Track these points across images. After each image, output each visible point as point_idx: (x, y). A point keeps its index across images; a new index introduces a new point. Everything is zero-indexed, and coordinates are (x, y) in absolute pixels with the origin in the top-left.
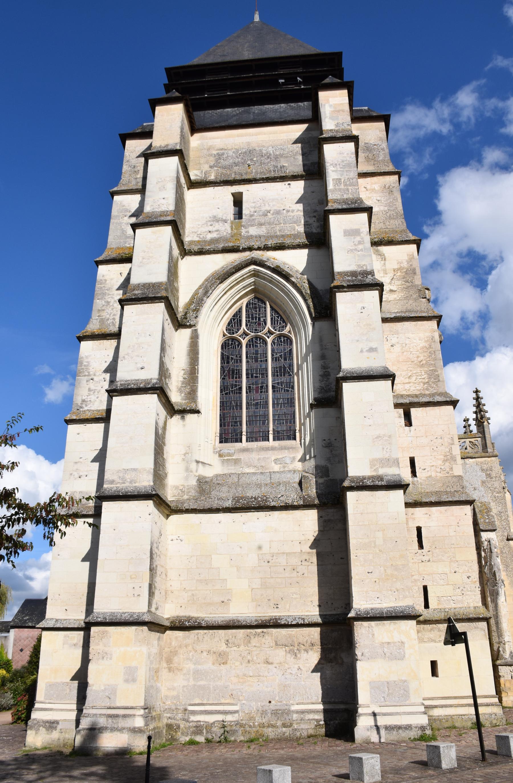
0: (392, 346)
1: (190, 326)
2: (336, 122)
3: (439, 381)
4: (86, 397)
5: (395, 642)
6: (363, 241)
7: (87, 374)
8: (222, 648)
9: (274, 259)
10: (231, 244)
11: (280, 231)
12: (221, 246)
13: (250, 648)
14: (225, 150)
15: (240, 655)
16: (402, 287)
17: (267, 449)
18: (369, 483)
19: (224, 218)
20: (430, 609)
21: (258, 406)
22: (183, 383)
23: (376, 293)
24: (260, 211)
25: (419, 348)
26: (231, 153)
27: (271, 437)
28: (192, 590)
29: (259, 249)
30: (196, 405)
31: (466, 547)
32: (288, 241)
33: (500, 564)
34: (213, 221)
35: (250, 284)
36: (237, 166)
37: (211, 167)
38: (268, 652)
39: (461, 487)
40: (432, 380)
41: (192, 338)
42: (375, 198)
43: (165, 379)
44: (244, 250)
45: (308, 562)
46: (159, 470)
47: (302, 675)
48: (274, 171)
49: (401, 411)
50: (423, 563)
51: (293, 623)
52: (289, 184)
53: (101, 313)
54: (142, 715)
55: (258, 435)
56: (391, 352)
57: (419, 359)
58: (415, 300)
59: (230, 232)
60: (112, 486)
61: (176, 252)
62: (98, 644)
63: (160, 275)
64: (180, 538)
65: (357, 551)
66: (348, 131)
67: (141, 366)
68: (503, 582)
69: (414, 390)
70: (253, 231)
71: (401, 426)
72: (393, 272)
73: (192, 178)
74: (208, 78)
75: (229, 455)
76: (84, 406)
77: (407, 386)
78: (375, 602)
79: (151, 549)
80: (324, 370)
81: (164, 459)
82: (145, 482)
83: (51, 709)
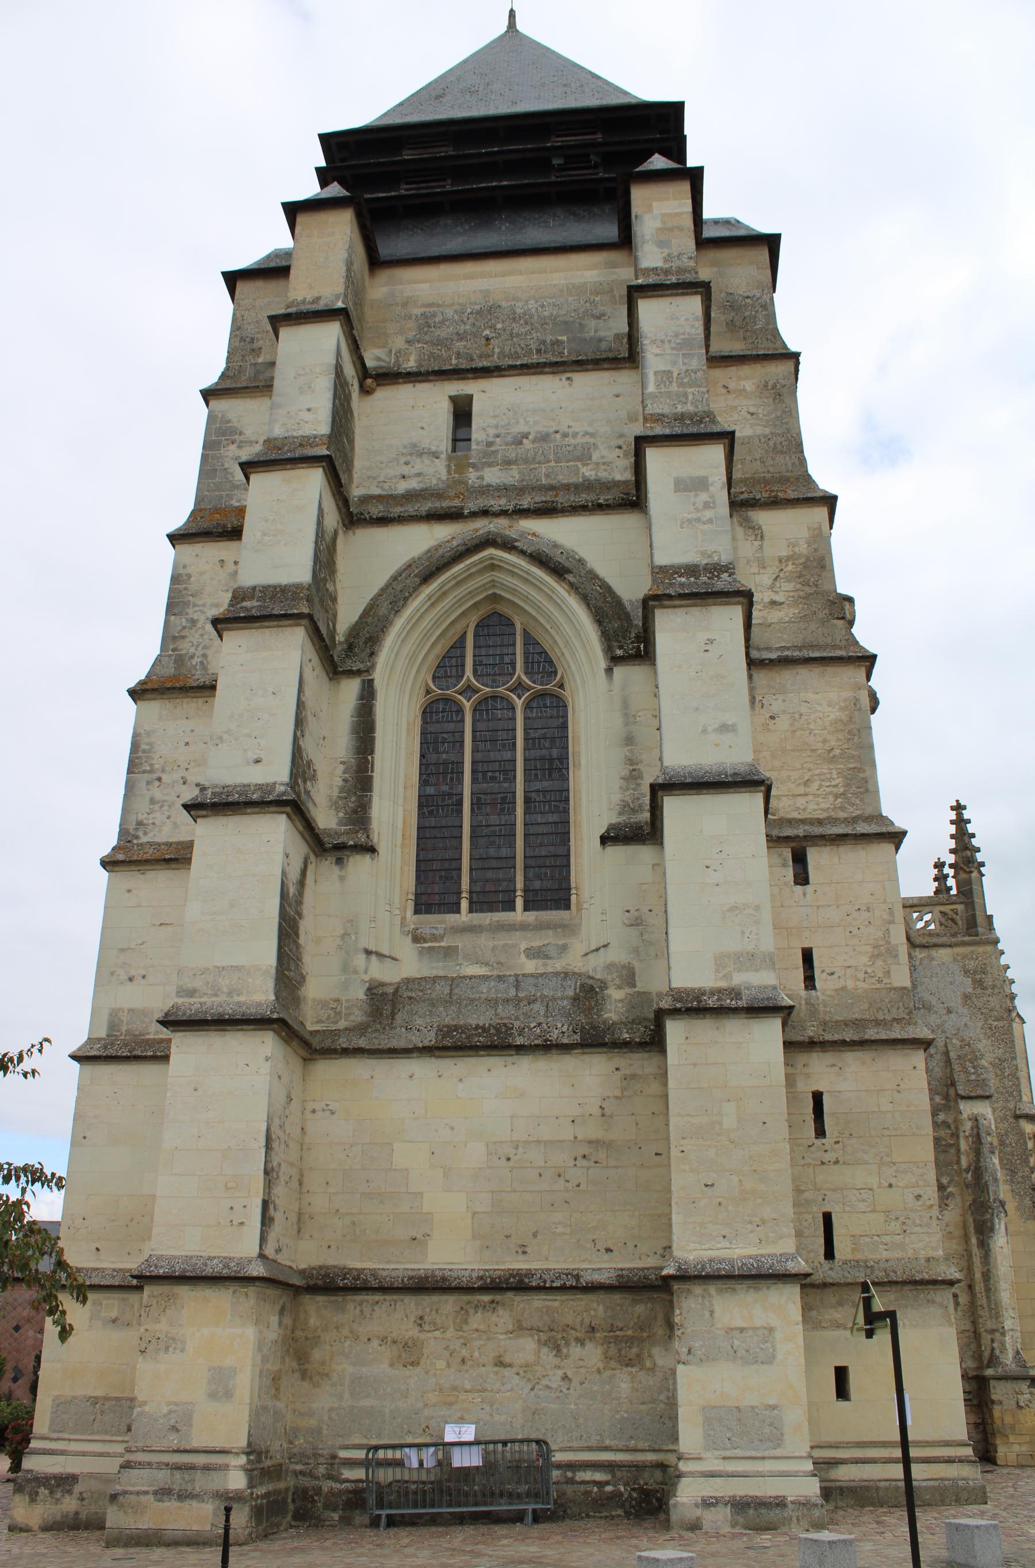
0: (772, 718)
1: (359, 672)
2: (666, 251)
3: (867, 791)
4: (145, 815)
5: (757, 1328)
6: (714, 503)
7: (148, 768)
8: (411, 1333)
9: (534, 534)
10: (446, 504)
11: (547, 476)
12: (425, 507)
13: (465, 1334)
14: (439, 306)
15: (447, 1348)
16: (796, 594)
17: (512, 928)
18: (711, 1002)
19: (434, 449)
20: (836, 1260)
21: (492, 836)
22: (342, 790)
23: (736, 613)
24: (508, 434)
25: (827, 724)
26: (449, 313)
27: (519, 903)
28: (353, 1214)
29: (504, 513)
30: (368, 837)
31: (914, 1134)
32: (563, 499)
33: (998, 1167)
34: (411, 454)
35: (484, 585)
36: (461, 339)
37: (409, 342)
38: (503, 1343)
39: (907, 1011)
40: (854, 789)
41: (362, 697)
42: (745, 409)
43: (305, 782)
44: (474, 515)
45: (589, 1160)
46: (289, 970)
47: (572, 1391)
48: (539, 351)
49: (788, 854)
50: (824, 1167)
51: (554, 1285)
52: (568, 379)
53: (178, 643)
54: (241, 1466)
55: (492, 898)
56: (769, 730)
57: (827, 746)
58: (823, 622)
59: (445, 478)
60: (192, 1000)
61: (332, 519)
62: (158, 1321)
63: (297, 569)
64: (330, 1108)
65: (683, 1142)
66: (689, 272)
67: (255, 757)
68: (1002, 1204)
69: (815, 810)
70: (493, 476)
71: (786, 884)
72: (777, 563)
73: (370, 363)
74: (407, 155)
75: (434, 938)
76: (140, 834)
77: (801, 802)
78: (719, 1246)
79: (268, 1130)
80: (631, 768)
81: (298, 946)
82: (261, 994)
83: (63, 1453)
